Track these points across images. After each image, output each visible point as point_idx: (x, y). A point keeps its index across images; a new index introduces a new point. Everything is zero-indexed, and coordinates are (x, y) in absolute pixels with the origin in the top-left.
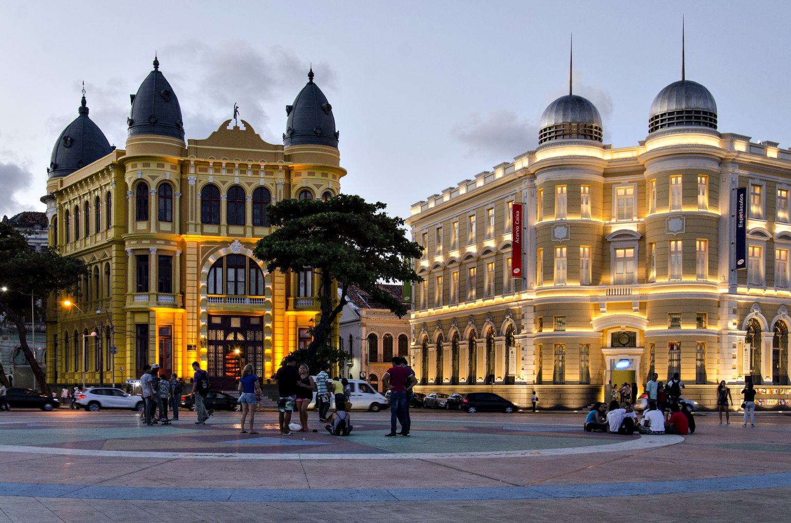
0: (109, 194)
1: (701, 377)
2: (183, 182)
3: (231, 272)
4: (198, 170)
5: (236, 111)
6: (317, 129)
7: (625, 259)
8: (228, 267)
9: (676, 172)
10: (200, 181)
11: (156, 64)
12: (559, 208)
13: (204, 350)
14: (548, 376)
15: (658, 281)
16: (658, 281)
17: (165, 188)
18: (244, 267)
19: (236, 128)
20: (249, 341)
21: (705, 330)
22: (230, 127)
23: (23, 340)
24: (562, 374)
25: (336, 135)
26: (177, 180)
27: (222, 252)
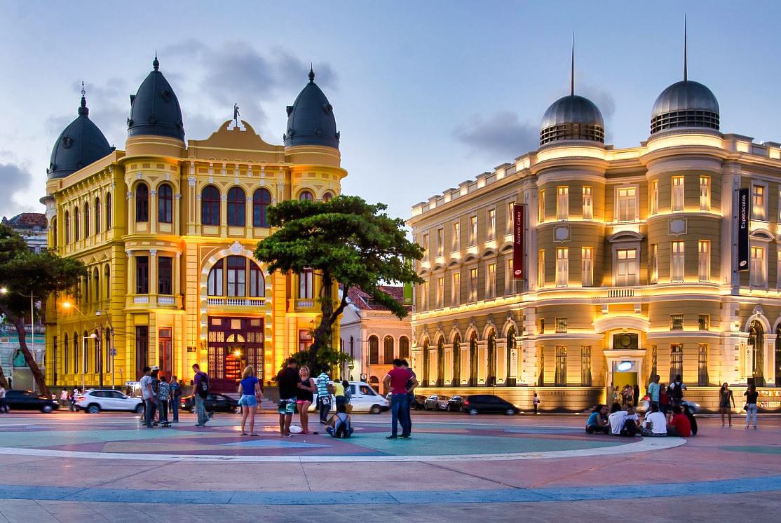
0: (109, 195)
1: (704, 379)
2: (183, 183)
3: (232, 273)
4: (198, 171)
6: (318, 129)
7: (627, 260)
9: (678, 173)
10: (200, 182)
14: (549, 378)
15: (660, 282)
16: (660, 282)
17: (165, 189)
20: (249, 343)
21: (706, 332)
23: (22, 342)
24: (564, 376)
25: (337, 136)
26: (177, 181)
27: (223, 254)
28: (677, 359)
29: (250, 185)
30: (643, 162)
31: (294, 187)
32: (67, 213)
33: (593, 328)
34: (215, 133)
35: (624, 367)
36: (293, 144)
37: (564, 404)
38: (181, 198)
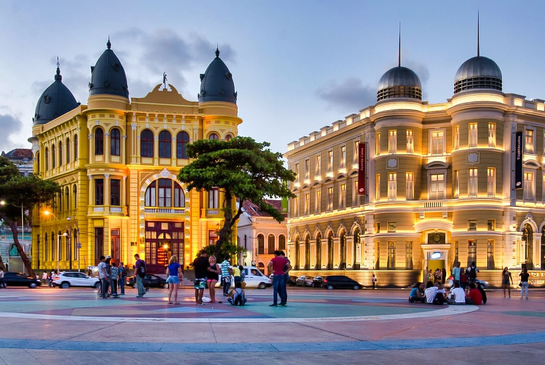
0: (76, 136)
1: (491, 265)
2: (128, 128)
3: (162, 191)
4: (138, 119)
5: (165, 78)
7: (437, 182)
8: (159, 187)
9: (473, 121)
10: (140, 127)
11: (109, 45)
12: (391, 146)
13: (143, 246)
14: (383, 264)
15: (461, 197)
16: (461, 197)
17: (115, 132)
18: (170, 187)
19: (165, 90)
20: (174, 239)
21: (493, 232)
22: (161, 89)
23: (16, 239)
24: (393, 263)
25: (235, 95)
26: (124, 126)
27: (155, 177)
28: (473, 250)
29: (156, 128)
30: (449, 113)
31: (206, 130)
32: (47, 149)
33: (414, 229)
34: (150, 93)
35: (436, 256)
36: (204, 100)
37: (394, 282)
38: (126, 138)
